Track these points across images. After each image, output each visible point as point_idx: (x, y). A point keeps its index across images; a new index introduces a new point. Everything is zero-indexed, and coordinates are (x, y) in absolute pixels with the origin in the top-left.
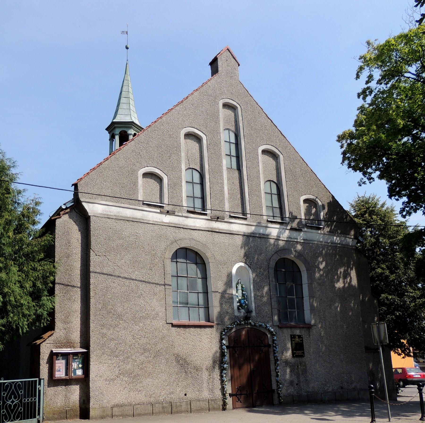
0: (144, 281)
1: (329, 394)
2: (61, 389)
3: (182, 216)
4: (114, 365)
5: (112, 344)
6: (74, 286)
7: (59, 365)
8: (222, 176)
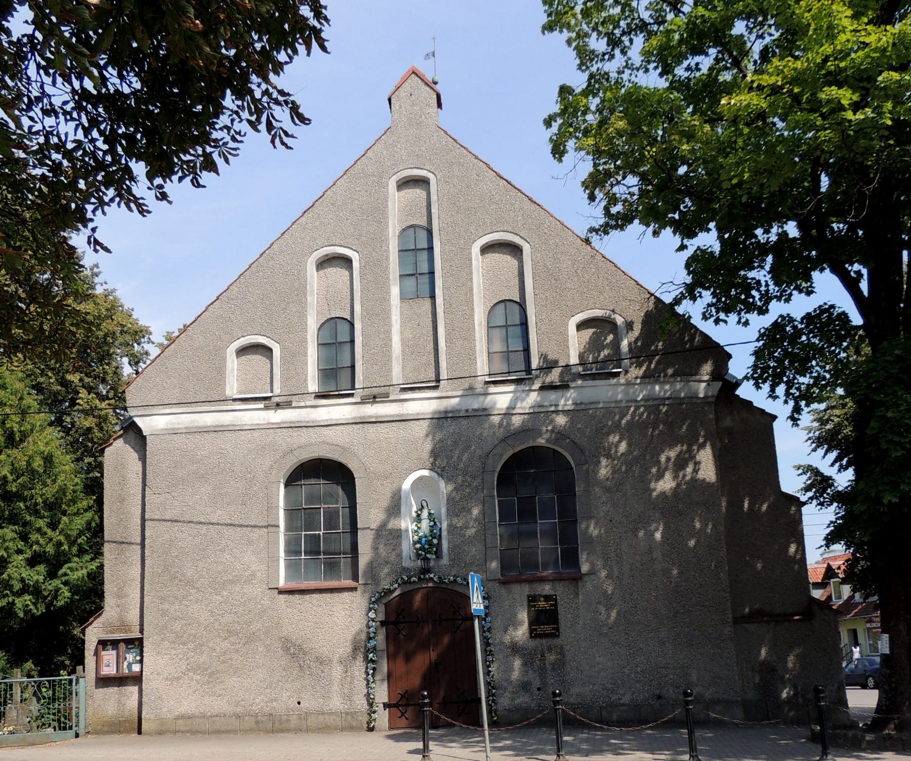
0: (231, 525)
1: (622, 708)
2: (112, 691)
3: (306, 407)
4: (180, 656)
5: (177, 626)
6: (131, 543)
7: (108, 657)
8: (389, 318)
